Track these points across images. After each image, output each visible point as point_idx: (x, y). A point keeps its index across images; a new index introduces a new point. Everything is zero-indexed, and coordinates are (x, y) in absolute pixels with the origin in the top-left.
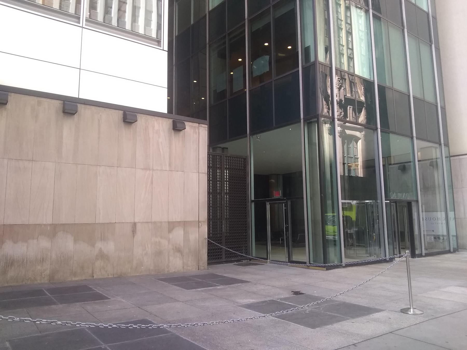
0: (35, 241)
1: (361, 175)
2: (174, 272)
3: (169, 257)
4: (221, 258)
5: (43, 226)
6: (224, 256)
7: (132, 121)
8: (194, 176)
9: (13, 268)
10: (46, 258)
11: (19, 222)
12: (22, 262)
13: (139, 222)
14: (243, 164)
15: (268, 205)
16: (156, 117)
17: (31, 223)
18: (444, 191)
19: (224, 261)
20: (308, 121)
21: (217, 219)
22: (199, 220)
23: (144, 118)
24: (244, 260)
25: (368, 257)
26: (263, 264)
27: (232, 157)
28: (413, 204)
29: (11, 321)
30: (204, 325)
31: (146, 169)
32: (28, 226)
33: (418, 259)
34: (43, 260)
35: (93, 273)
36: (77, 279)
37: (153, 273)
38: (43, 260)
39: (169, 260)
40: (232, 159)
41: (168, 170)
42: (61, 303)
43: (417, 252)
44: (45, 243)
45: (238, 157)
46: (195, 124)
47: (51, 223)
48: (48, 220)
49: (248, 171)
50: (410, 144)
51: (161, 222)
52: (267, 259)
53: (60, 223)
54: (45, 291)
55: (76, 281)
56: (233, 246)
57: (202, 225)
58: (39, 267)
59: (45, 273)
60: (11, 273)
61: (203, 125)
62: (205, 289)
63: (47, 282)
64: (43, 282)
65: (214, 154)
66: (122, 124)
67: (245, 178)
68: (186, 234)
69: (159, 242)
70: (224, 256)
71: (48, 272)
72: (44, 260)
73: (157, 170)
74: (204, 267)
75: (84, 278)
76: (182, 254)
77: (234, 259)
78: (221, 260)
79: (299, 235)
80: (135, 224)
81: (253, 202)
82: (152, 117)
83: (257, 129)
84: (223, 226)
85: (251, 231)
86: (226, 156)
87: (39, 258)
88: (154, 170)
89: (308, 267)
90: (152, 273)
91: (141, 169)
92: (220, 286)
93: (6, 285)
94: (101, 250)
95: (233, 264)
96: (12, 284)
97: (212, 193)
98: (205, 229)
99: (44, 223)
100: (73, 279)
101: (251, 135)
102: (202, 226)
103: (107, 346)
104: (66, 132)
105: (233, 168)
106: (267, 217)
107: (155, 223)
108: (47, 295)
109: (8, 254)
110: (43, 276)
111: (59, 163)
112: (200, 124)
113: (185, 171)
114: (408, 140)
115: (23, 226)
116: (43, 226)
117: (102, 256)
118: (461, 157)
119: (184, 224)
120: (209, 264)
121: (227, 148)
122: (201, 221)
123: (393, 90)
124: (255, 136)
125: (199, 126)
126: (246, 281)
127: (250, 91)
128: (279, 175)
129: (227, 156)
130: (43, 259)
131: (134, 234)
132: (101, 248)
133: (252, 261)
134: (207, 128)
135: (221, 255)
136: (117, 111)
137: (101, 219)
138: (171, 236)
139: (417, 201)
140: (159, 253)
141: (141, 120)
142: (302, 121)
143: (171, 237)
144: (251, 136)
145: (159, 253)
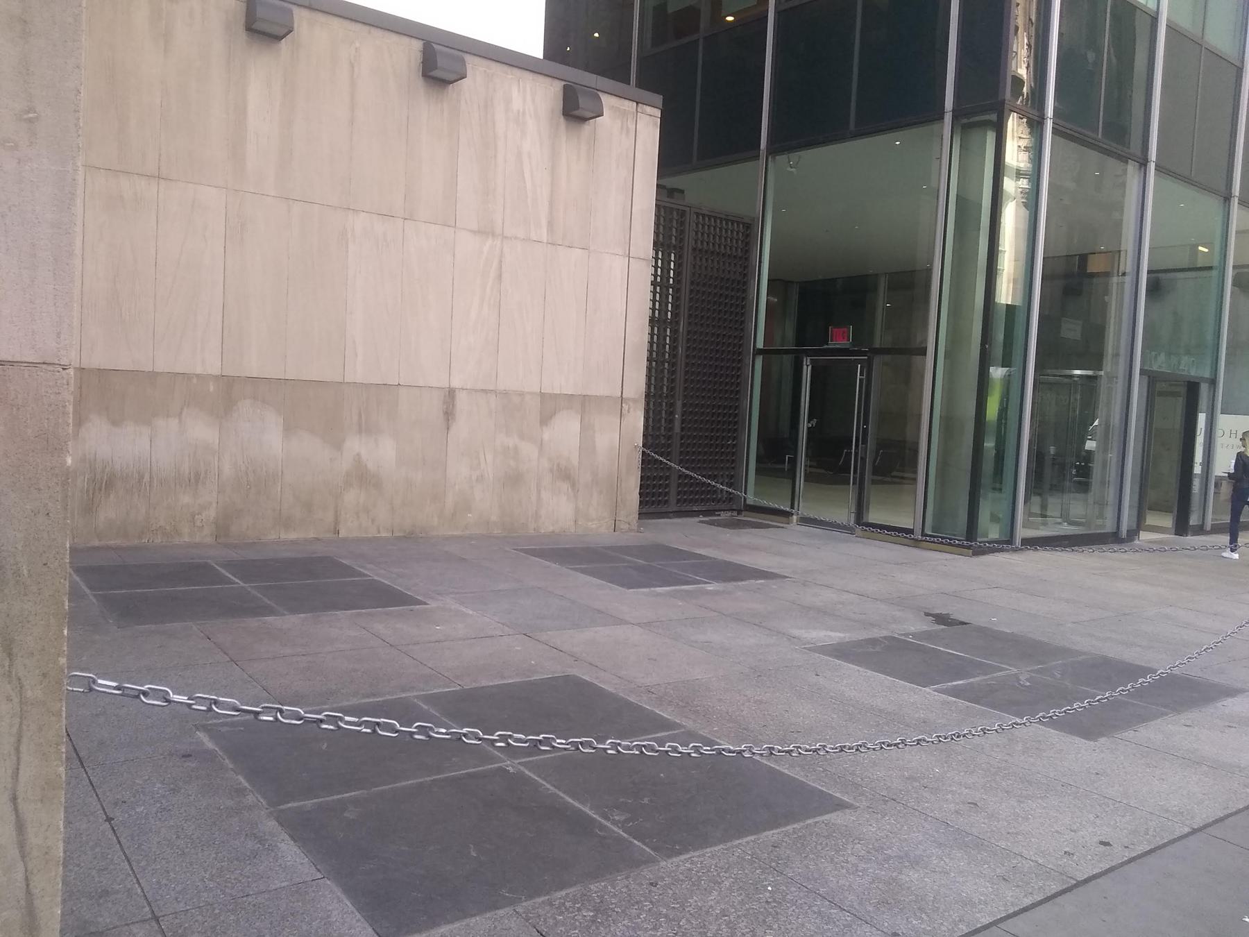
0: (174, 423)
1: (1007, 299)
2: (553, 532)
3: (539, 492)
4: (666, 502)
5: (195, 381)
6: (673, 497)
7: (451, 77)
8: (619, 264)
9: (112, 496)
10: (206, 473)
11: (124, 363)
12: (137, 480)
13: (463, 389)
14: (742, 241)
15: (807, 366)
16: (516, 71)
17: (161, 366)
18: (1215, 362)
19: (674, 510)
20: (965, 121)
21: (660, 396)
22: (624, 397)
23: (481, 69)
24: (724, 510)
25: (1060, 523)
26: (781, 525)
27: (713, 217)
28: (1204, 388)
29: (422, 740)
30: (917, 744)
31: (485, 232)
32: (153, 376)
33: (1192, 537)
34: (197, 481)
35: (337, 522)
36: (292, 536)
37: (496, 532)
38: (195, 480)
39: (539, 498)
40: (718, 225)
41: (545, 241)
42: (293, 611)
43: (1194, 520)
44: (201, 430)
45: (730, 218)
46: (627, 103)
47: (215, 371)
48: (210, 363)
49: (754, 263)
50: (1219, 219)
51: (521, 394)
52: (787, 514)
53: (243, 375)
54: (216, 566)
55: (294, 542)
56: (710, 473)
57: (629, 409)
58: (186, 499)
59: (204, 515)
60: (109, 512)
61: (648, 109)
62: (675, 590)
63: (209, 540)
64: (197, 540)
65: (673, 206)
66: (420, 82)
67: (745, 283)
68: (586, 428)
69: (516, 449)
70: (673, 497)
71: (212, 513)
72: (201, 478)
73: (516, 238)
74: (629, 524)
75: (312, 536)
76: (573, 485)
77: (700, 508)
78: (664, 509)
79: (845, 450)
80: (451, 393)
81: (760, 354)
82: (506, 68)
83: (785, 141)
84: (677, 416)
85: (749, 436)
86: (697, 214)
87: (187, 472)
88: (506, 237)
89: (916, 544)
90: (496, 532)
91: (471, 231)
92: (710, 583)
93: (96, 543)
94: (358, 458)
95: (697, 519)
96: (112, 542)
97: (671, 323)
98: (636, 420)
99: (199, 371)
100: (283, 536)
101: (770, 154)
102: (629, 412)
103: (519, 763)
104: (255, 94)
105: (726, 253)
106: (803, 400)
107: (505, 394)
108: (226, 583)
109: (96, 454)
110: (198, 523)
111: (236, 190)
112: (640, 105)
113: (592, 248)
114: (1212, 204)
115: (134, 376)
116: (195, 381)
117: (363, 476)
118: (1172, 275)
119: (584, 403)
120: (642, 515)
121: (682, 192)
122: (629, 399)
123: (1203, 48)
124: (782, 159)
125: (637, 112)
126: (772, 573)
127: (779, 12)
128: (792, 282)
129: (701, 212)
130: (197, 475)
131: (450, 422)
132: (358, 455)
133: (743, 515)
134: (659, 119)
135: (666, 494)
136: (406, 40)
137: (358, 372)
138: (546, 435)
139: (1213, 382)
140: (514, 480)
141: (477, 71)
142: (948, 118)
143: (546, 436)
144: (770, 159)
145: (514, 480)
